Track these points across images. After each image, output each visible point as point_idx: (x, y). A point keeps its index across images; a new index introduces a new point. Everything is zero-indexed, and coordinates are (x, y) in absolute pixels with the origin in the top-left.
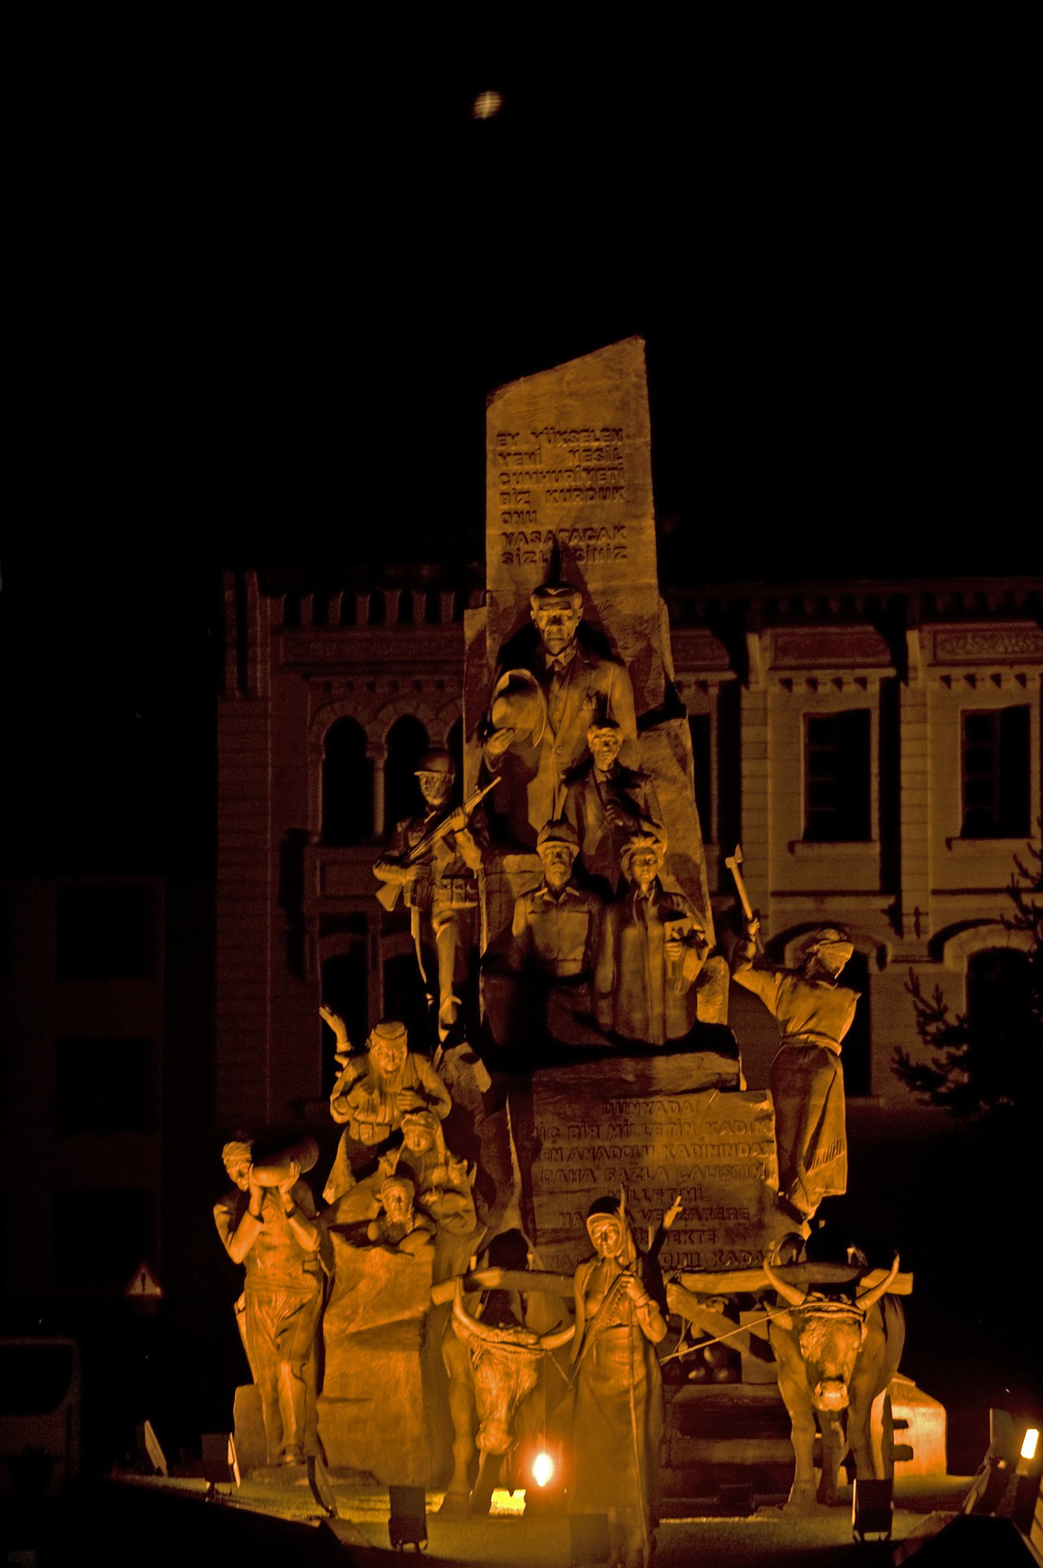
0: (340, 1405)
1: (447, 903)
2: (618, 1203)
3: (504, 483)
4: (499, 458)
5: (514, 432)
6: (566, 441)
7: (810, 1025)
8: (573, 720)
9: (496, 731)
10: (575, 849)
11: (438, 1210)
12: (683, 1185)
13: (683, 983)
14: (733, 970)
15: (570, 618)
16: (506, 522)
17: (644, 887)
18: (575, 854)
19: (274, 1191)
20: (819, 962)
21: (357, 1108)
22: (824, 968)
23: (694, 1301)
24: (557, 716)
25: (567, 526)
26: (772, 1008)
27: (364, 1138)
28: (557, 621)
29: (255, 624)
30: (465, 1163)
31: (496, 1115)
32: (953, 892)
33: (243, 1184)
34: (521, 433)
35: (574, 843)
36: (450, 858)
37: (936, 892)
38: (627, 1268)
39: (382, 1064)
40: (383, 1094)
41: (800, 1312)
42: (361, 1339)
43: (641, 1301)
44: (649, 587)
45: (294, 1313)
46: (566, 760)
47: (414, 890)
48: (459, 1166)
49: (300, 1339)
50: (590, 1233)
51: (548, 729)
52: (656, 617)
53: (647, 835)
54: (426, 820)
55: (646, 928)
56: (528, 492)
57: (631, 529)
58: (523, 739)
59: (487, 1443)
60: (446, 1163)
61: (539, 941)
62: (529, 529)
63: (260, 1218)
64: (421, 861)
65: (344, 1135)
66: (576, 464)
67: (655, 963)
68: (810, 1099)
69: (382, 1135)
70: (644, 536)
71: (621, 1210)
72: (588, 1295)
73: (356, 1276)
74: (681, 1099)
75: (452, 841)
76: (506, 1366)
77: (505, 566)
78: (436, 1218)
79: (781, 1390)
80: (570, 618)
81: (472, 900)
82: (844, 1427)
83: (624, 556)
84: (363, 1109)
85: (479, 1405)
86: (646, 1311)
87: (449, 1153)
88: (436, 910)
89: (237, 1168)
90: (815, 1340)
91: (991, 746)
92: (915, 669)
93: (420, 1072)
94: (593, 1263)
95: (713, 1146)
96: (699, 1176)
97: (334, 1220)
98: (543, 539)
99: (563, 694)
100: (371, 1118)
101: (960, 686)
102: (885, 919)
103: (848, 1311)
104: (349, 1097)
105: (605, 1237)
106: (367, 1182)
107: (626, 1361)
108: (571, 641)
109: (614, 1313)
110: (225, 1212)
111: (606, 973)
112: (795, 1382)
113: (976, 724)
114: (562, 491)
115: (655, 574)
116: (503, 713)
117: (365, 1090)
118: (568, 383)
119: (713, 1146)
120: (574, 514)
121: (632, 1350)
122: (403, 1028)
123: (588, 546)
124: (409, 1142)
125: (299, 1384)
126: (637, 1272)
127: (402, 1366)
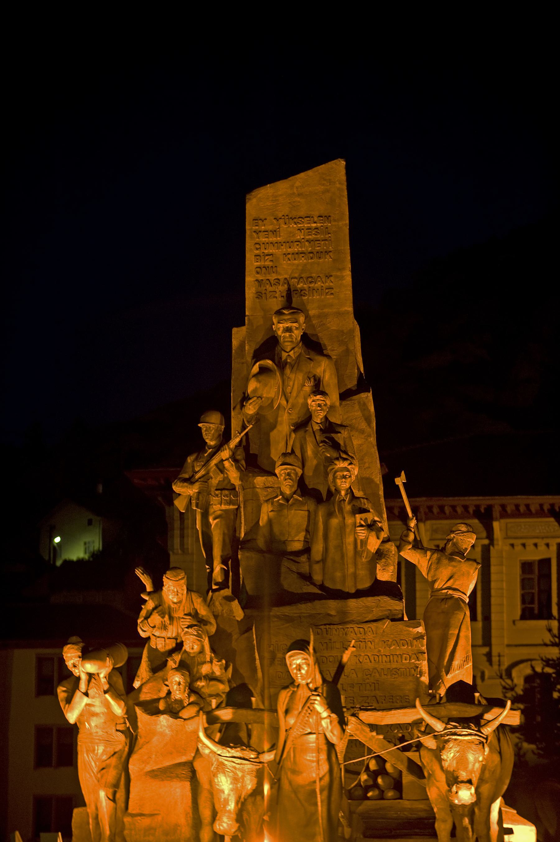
0: (139, 818)
1: (218, 507)
2: (308, 643)
3: (257, 249)
4: (254, 234)
5: (263, 218)
6: (295, 223)
7: (449, 584)
8: (299, 392)
9: (250, 399)
10: (300, 472)
11: (206, 691)
12: (367, 681)
13: (367, 553)
14: (399, 548)
15: (297, 328)
16: (258, 273)
17: (343, 493)
18: (300, 474)
19: (96, 677)
20: (455, 544)
21: (154, 627)
22: (457, 548)
23: (367, 729)
24: (289, 389)
25: (296, 275)
26: (424, 574)
27: (160, 647)
28: (288, 330)
29: (188, 519)
30: (224, 661)
31: (246, 635)
32: (516, 646)
33: (76, 672)
34: (268, 218)
35: (299, 468)
36: (220, 477)
37: (508, 646)
38: (316, 689)
39: (170, 597)
40: (171, 618)
41: (442, 736)
42: (155, 774)
43: (325, 714)
44: (348, 312)
45: (110, 758)
46: (295, 417)
47: (198, 499)
48: (220, 663)
49: (111, 775)
50: (288, 665)
51: (283, 398)
52: (352, 331)
53: (345, 459)
54: (206, 455)
55: (344, 518)
56: (272, 255)
57: (337, 277)
58: (267, 404)
59: (221, 828)
60: (211, 662)
61: (276, 529)
62: (273, 277)
63: (86, 694)
64: (202, 479)
65: (147, 645)
66: (302, 237)
67: (350, 540)
68: (448, 630)
69: (171, 644)
70: (344, 282)
71: (311, 648)
72: (287, 712)
73: (153, 733)
74: (366, 626)
75: (221, 467)
76: (236, 774)
77: (257, 300)
78: (204, 697)
79: (429, 794)
80: (297, 328)
81: (233, 505)
82: (472, 822)
83: (332, 294)
84: (158, 628)
85: (216, 802)
86: (328, 721)
87: (213, 655)
88: (211, 511)
89: (72, 662)
90: (452, 755)
91: (535, 575)
92: (498, 540)
93: (195, 604)
94: (292, 689)
95: (386, 656)
96: (377, 674)
97: (138, 697)
98: (281, 283)
99: (292, 376)
100: (164, 634)
101: (519, 548)
102: (485, 658)
103: (476, 735)
104: (149, 620)
105: (299, 668)
106: (160, 674)
107: (315, 759)
108: (298, 344)
109: (307, 723)
110: (64, 691)
111: (318, 548)
112: (438, 788)
113: (526, 567)
114: (293, 254)
115: (352, 304)
116: (254, 386)
117: (159, 615)
118: (297, 188)
119: (386, 656)
120: (300, 268)
121: (318, 751)
122: (184, 574)
123: (310, 287)
124: (187, 647)
125: (112, 803)
126: (322, 693)
127: (180, 790)
